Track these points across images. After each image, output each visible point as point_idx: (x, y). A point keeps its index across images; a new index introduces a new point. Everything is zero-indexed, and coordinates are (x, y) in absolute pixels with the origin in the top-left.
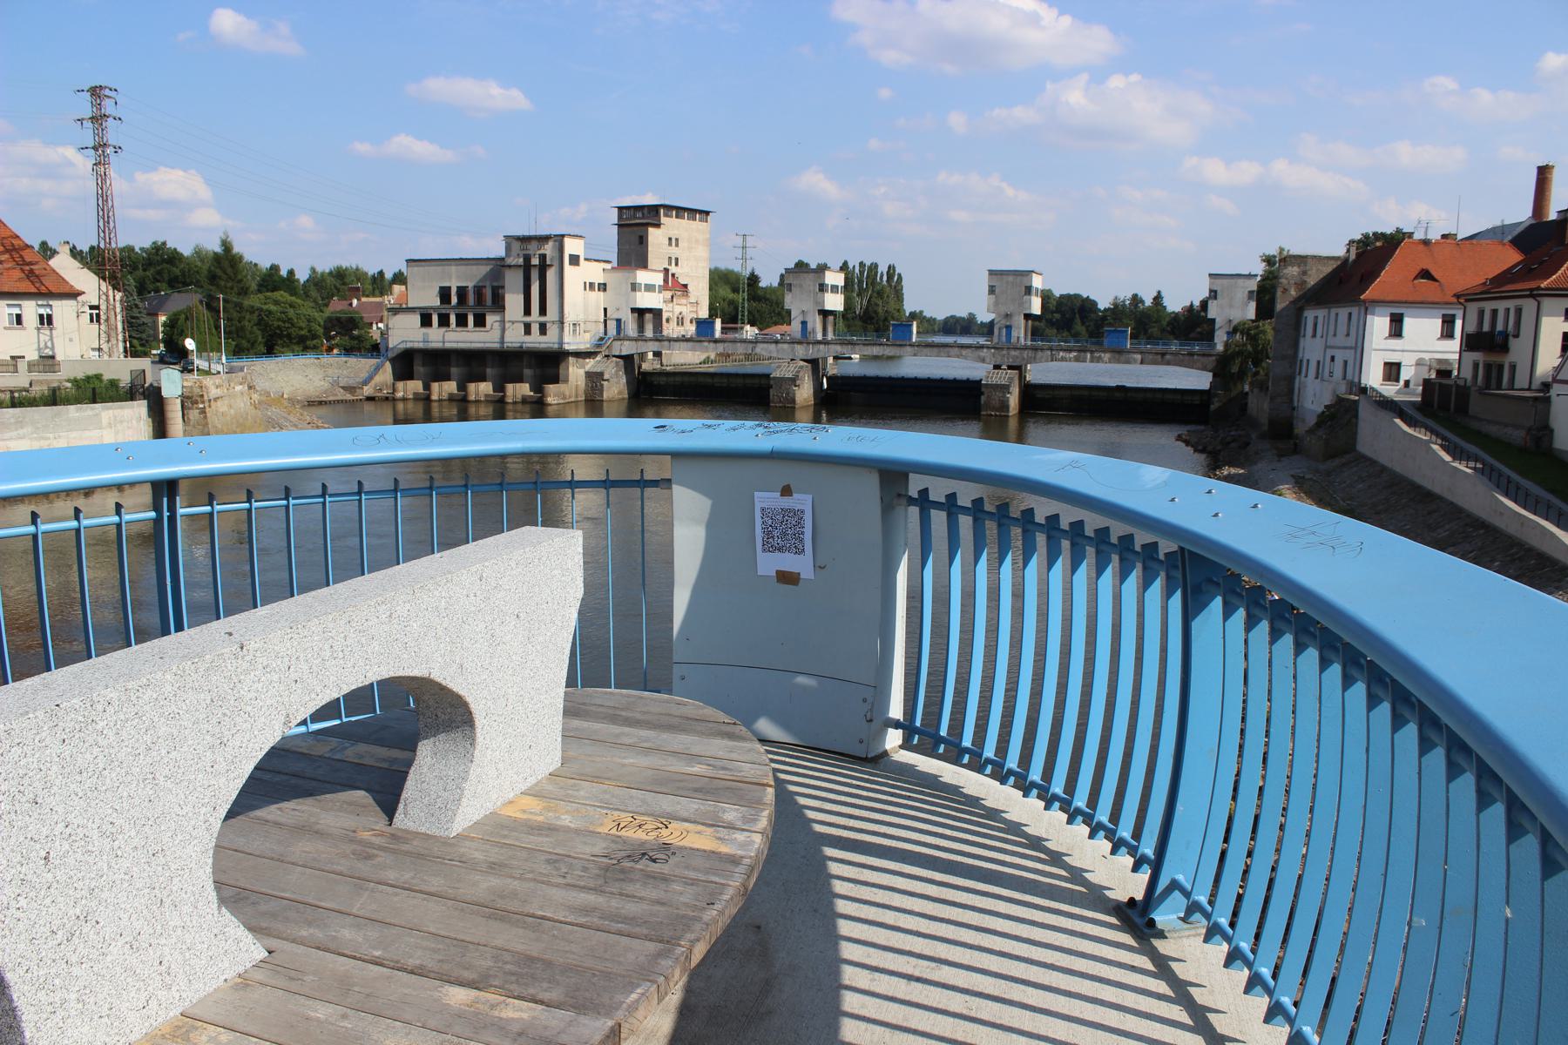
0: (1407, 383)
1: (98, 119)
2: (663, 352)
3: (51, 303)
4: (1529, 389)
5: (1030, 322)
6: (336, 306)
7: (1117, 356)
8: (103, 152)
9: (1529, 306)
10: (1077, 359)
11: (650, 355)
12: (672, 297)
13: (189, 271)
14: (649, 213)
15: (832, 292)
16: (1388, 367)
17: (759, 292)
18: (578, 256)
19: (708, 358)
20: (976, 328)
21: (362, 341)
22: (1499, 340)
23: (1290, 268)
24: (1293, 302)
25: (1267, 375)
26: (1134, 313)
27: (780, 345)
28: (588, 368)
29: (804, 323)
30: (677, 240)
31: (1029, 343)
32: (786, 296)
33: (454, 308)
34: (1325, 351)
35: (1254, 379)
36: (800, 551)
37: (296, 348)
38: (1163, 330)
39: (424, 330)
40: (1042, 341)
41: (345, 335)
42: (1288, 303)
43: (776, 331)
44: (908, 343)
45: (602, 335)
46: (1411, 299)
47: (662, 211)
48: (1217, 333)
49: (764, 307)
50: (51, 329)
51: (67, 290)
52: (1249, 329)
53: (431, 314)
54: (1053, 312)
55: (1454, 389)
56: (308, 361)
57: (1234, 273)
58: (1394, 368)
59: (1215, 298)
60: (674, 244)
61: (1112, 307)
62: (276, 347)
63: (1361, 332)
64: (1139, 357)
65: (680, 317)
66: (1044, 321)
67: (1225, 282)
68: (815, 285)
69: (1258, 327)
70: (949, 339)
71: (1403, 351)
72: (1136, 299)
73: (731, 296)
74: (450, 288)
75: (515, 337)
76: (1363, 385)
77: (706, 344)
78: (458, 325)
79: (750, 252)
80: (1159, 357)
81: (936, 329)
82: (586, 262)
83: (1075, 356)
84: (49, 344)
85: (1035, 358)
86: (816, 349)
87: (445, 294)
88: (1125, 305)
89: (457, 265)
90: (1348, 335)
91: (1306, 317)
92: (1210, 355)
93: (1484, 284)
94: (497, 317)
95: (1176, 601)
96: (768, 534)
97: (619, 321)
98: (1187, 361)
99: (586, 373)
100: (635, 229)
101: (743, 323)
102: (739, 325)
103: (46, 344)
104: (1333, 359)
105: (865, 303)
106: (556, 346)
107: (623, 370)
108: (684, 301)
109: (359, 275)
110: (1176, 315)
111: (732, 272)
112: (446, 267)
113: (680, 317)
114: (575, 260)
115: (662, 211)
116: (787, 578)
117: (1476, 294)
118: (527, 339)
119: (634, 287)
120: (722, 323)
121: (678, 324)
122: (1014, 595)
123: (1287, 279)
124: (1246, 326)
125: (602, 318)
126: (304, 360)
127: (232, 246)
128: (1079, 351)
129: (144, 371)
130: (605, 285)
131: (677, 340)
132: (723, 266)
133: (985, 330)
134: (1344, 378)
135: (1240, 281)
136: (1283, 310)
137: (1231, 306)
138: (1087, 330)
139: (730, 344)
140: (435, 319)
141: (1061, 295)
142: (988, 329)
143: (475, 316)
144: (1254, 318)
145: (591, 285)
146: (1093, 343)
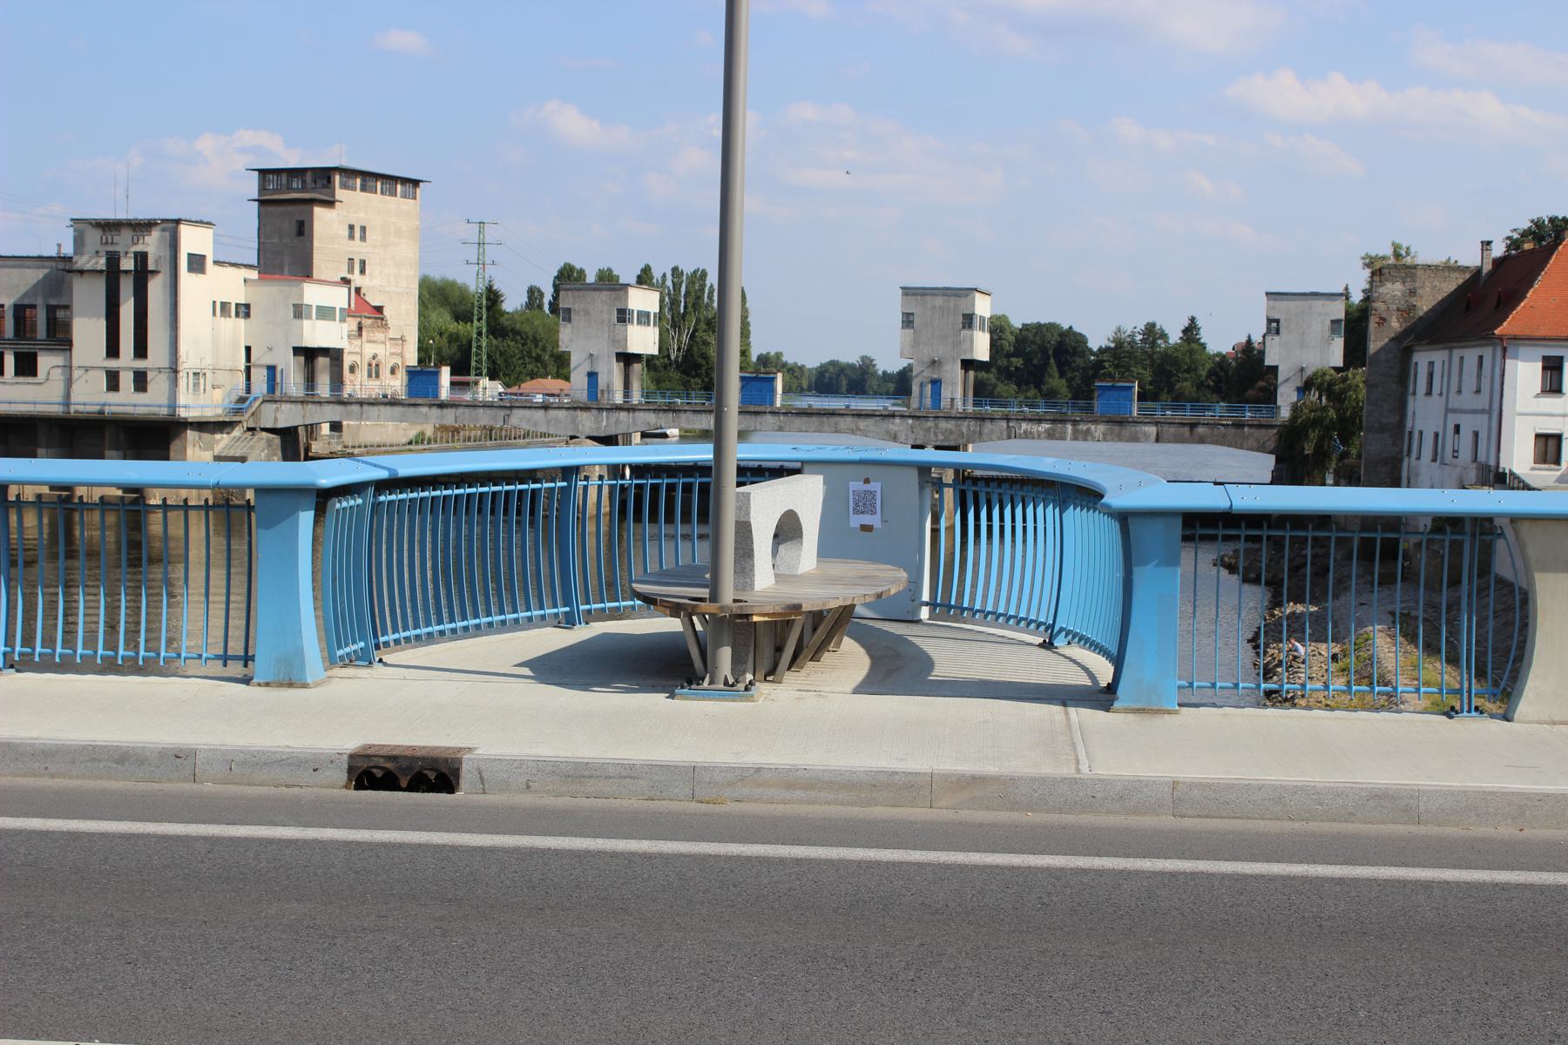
2: (345, 423)
5: (971, 373)
7: (1116, 428)
10: (1050, 435)
11: (325, 429)
12: (360, 329)
15: (639, 322)
16: (1542, 441)
18: (203, 257)
19: (423, 434)
20: (874, 383)
23: (1389, 285)
24: (1398, 339)
25: (1359, 456)
26: (1150, 357)
27: (551, 412)
29: (592, 376)
30: (363, 229)
31: (970, 408)
32: (562, 330)
35: (1341, 464)
36: (874, 513)
38: (1200, 385)
42: (1387, 340)
43: (538, 389)
44: (769, 410)
45: (242, 393)
47: (337, 178)
48: (1280, 390)
49: (511, 345)
52: (1331, 384)
54: (1009, 356)
57: (1308, 291)
58: (1552, 443)
61: (1112, 345)
64: (1152, 430)
66: (993, 370)
67: (1294, 305)
69: (1345, 379)
72: (1151, 332)
73: (453, 327)
75: (90, 396)
76: (1501, 470)
77: (424, 410)
79: (491, 253)
80: (1186, 430)
81: (805, 384)
82: (218, 268)
83: (1047, 431)
86: (613, 420)
88: (1134, 341)
90: (1478, 391)
91: (1416, 363)
92: (1271, 427)
95: (1057, 510)
96: (856, 504)
97: (272, 369)
100: (290, 208)
101: (480, 374)
102: (472, 378)
104: (1457, 429)
105: (685, 338)
106: (164, 411)
108: (379, 336)
110: (1223, 357)
114: (197, 263)
116: (866, 528)
118: (113, 397)
119: (299, 311)
120: (453, 373)
121: (370, 376)
122: (983, 596)
124: (1328, 378)
125: (242, 364)
128: (1054, 421)
130: (247, 306)
131: (373, 403)
132: (437, 274)
133: (891, 387)
134: (1475, 459)
135: (1318, 304)
137: (1302, 345)
138: (1069, 387)
139: (467, 410)
141: (1026, 327)
142: (900, 384)
143: (18, 356)
144: (1340, 363)
145: (224, 306)
146: (1082, 409)
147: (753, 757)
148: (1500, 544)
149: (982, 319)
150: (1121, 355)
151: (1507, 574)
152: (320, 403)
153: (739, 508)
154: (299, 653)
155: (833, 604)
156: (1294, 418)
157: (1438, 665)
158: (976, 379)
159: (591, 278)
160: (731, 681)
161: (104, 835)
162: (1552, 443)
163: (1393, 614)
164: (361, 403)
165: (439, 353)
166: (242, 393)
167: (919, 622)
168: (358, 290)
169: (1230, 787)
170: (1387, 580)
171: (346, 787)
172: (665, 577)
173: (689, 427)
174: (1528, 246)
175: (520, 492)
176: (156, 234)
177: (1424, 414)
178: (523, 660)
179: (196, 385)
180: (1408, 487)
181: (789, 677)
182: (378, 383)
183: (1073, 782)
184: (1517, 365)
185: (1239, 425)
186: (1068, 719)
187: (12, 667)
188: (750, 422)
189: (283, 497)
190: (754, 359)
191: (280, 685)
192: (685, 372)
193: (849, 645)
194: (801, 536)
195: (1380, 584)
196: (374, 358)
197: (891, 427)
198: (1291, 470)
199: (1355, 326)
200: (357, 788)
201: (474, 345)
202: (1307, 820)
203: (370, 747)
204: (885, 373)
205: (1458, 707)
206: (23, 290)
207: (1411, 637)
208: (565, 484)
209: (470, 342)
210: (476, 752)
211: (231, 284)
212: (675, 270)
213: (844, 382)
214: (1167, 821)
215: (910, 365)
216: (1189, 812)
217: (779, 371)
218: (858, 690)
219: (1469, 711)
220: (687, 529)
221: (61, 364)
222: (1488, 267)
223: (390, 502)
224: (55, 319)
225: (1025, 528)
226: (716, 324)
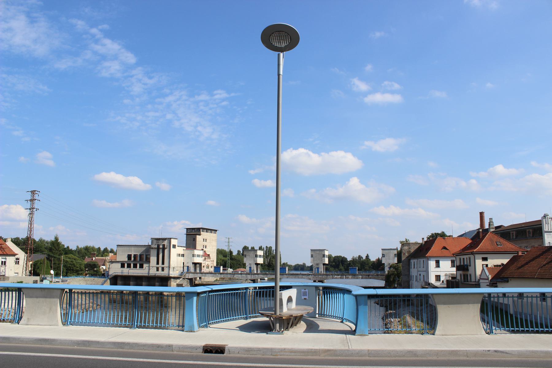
0: (443, 281)
1: (32, 200)
2: (202, 277)
3: (7, 257)
4: (475, 282)
6: (87, 260)
7: (354, 276)
8: (33, 210)
9: (472, 257)
10: (341, 278)
11: (198, 278)
12: (205, 259)
13: (38, 246)
14: (197, 231)
16: (436, 277)
19: (217, 279)
20: (306, 268)
21: (98, 272)
22: (466, 267)
24: (407, 257)
25: (402, 281)
27: (242, 275)
28: (177, 283)
29: (250, 268)
30: (206, 239)
31: (325, 273)
33: (132, 261)
36: (307, 296)
37: (75, 274)
38: (370, 267)
39: (122, 269)
41: (92, 270)
43: (240, 270)
44: (285, 274)
45: (182, 272)
46: (441, 256)
47: (201, 230)
48: (385, 268)
49: (234, 262)
50: (5, 266)
51: (12, 253)
52: (395, 266)
53: (125, 264)
54: (332, 262)
55: (455, 282)
56: (81, 279)
58: (438, 277)
59: (384, 257)
60: (205, 241)
62: (68, 274)
63: (427, 266)
67: (387, 251)
69: (398, 265)
70: (299, 272)
71: (440, 271)
73: (223, 258)
74: (131, 255)
75: (153, 272)
77: (217, 275)
80: (367, 276)
81: (292, 269)
84: (4, 271)
85: (327, 278)
87: (129, 257)
90: (424, 267)
93: (460, 251)
94: (147, 265)
95: (343, 295)
96: (303, 294)
97: (188, 267)
98: (377, 277)
99: (177, 284)
100: (192, 236)
101: (228, 268)
102: (227, 268)
103: (3, 271)
104: (420, 275)
105: (268, 260)
106: (167, 275)
108: (209, 260)
109: (93, 248)
111: (223, 250)
114: (174, 246)
115: (201, 230)
116: (305, 299)
117: (458, 254)
118: (157, 272)
119: (193, 256)
120: (223, 267)
121: (207, 268)
123: (404, 250)
124: (394, 265)
126: (79, 278)
127: (58, 239)
128: (341, 275)
129: (37, 280)
130: (184, 255)
131: (207, 273)
132: (220, 248)
133: (309, 269)
134: (424, 281)
135: (392, 251)
136: (405, 259)
137: (389, 259)
138: (344, 268)
140: (126, 265)
142: (311, 268)
143: (128, 264)
144: (397, 262)
145: (179, 254)
146: (347, 273)
147: (283, 346)
148: (430, 299)
149: (327, 255)
150: (354, 261)
151: (431, 303)
152: (197, 273)
153: (280, 296)
154: (193, 325)
155: (299, 315)
156: (388, 274)
157: (419, 322)
158: (326, 267)
159: (250, 249)
160: (279, 330)
161: (155, 363)
162: (438, 277)
163: (410, 312)
164: (205, 273)
165: (220, 263)
166: (182, 272)
167: (316, 317)
168: (205, 251)
169: (380, 351)
170: (408, 305)
171: (202, 353)
172: (265, 309)
173: (269, 278)
174: (431, 239)
175: (237, 292)
176: (167, 241)
177: (414, 272)
178: (238, 326)
179: (173, 270)
180: (411, 288)
181: (290, 329)
183: (348, 350)
184: (479, 303)
185: (377, 275)
186: (347, 337)
187: (137, 327)
188: (282, 276)
189: (190, 295)
190: (282, 264)
191: (189, 332)
192: (268, 267)
193: (302, 322)
194: (292, 301)
195: (407, 306)
197: (309, 277)
198: (389, 285)
199: (399, 255)
200: (205, 353)
201: (227, 262)
202: (395, 357)
203: (207, 344)
204: (308, 266)
205: (424, 333)
206: (141, 252)
207: (414, 317)
208: (245, 291)
209: (226, 261)
210: (228, 346)
211: (181, 250)
212: (266, 247)
213: (300, 268)
214: (367, 358)
215: (313, 265)
216: (372, 356)
217: (287, 266)
218: (304, 332)
219: (426, 333)
220: (270, 298)
221: (148, 266)
222: (424, 243)
223: (211, 295)
224: (147, 257)
225: (336, 297)
226: (275, 257)
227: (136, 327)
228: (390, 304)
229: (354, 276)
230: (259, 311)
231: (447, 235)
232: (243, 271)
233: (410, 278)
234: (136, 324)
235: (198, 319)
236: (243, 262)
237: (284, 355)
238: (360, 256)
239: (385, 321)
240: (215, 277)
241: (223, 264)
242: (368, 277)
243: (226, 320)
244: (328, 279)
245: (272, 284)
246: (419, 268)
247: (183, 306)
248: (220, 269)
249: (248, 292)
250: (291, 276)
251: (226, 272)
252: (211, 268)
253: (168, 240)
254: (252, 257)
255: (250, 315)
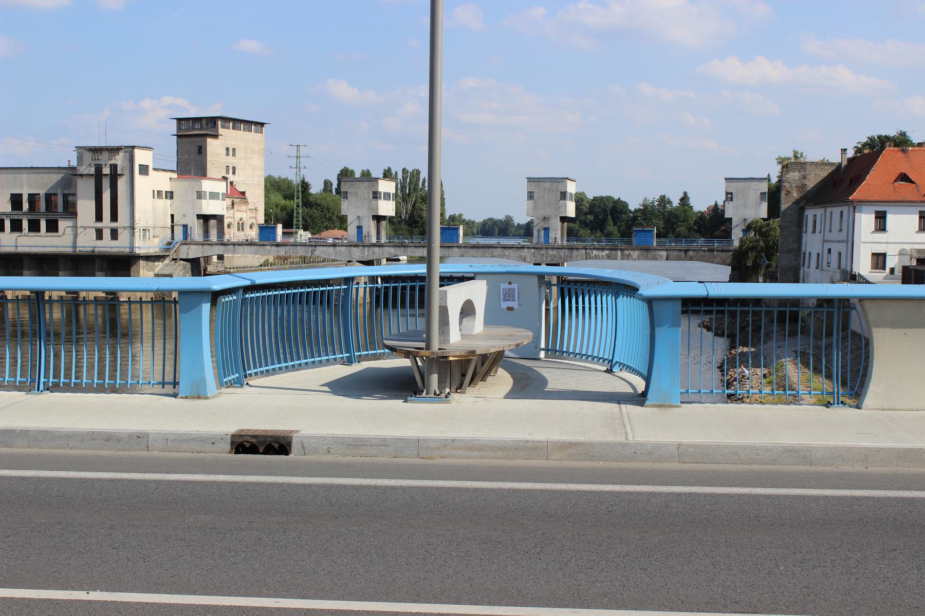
0: (892, 271)
2: (225, 255)
7: (645, 253)
10: (609, 257)
11: (215, 259)
12: (233, 204)
15: (385, 199)
16: (875, 257)
17: (310, 198)
19: (267, 261)
23: (792, 173)
24: (797, 202)
25: (777, 267)
27: (338, 248)
29: (359, 228)
30: (234, 150)
31: (565, 243)
33: (25, 214)
34: (823, 245)
35: (766, 271)
36: (514, 301)
38: (690, 229)
40: (577, 241)
42: (791, 203)
43: (330, 235)
44: (456, 245)
45: (169, 240)
46: (891, 199)
47: (220, 122)
48: (733, 231)
49: (315, 212)
52: (761, 228)
54: (586, 214)
57: (748, 177)
58: (881, 258)
61: (642, 208)
63: (851, 228)
64: (664, 253)
65: (241, 223)
67: (740, 185)
68: (369, 193)
69: (768, 225)
71: (887, 243)
72: (663, 200)
73: (283, 202)
74: (21, 195)
75: (87, 242)
76: (853, 273)
77: (269, 247)
78: (30, 230)
80: (683, 253)
81: (475, 231)
83: (607, 255)
87: (16, 201)
88: (654, 205)
89: (28, 173)
90: (841, 230)
91: (807, 216)
95: (614, 297)
96: (504, 296)
98: (708, 256)
100: (195, 139)
102: (294, 230)
105: (409, 207)
106: (127, 250)
107: (190, 272)
108: (244, 208)
111: (285, 180)
112: (18, 175)
113: (241, 223)
114: (144, 170)
116: (510, 309)
119: (200, 195)
120: (283, 228)
124: (759, 224)
128: (610, 249)
130: (172, 193)
132: (276, 174)
133: (522, 232)
134: (839, 267)
136: (788, 208)
138: (619, 231)
139: (291, 248)
142: (527, 230)
143: (48, 222)
144: (766, 216)
145: (159, 192)
146: (626, 243)
148: (854, 313)
149: (571, 194)
150: (646, 212)
151: (858, 330)
153: (441, 299)
154: (203, 381)
155: (493, 350)
156: (741, 246)
157: (820, 379)
159: (358, 175)
163: (796, 352)
164: (234, 244)
165: (276, 216)
167: (539, 359)
168: (232, 183)
170: (793, 334)
172: (401, 337)
174: (866, 151)
175: (322, 291)
176: (121, 154)
177: (812, 243)
179: (144, 236)
181: (469, 389)
182: (243, 233)
183: (624, 445)
185: (711, 251)
186: (621, 411)
187: (48, 389)
188: (446, 252)
189: (192, 296)
190: (447, 218)
191: (193, 398)
192: (410, 225)
193: (501, 372)
194: (475, 314)
195: (789, 336)
196: (241, 220)
198: (740, 274)
199: (773, 196)
200: (236, 453)
201: (295, 212)
203: (243, 430)
204: (518, 224)
205: (832, 402)
206: (50, 186)
207: (806, 364)
209: (293, 212)
211: (163, 181)
213: (497, 230)
217: (461, 224)
218: (507, 396)
219: (838, 404)
222: (845, 163)
223: (252, 298)
225: (596, 308)
226: (427, 199)
227: (44, 390)
228: (743, 328)
229: (646, 250)
230: (383, 339)
231: (914, 142)
232: (338, 239)
233: (802, 259)
234: (42, 380)
235: (216, 368)
236: (340, 212)
237: (450, 457)
238: (664, 196)
239: (727, 374)
240: (262, 255)
241: (283, 220)
242: (685, 254)
243: (293, 366)
244: (573, 258)
245: (421, 269)
246: (827, 233)
247: (174, 331)
248: (275, 233)
249: (354, 291)
250: (472, 251)
251: (292, 240)
252: (249, 229)
253: (126, 152)
254: (365, 199)
255: (360, 351)
